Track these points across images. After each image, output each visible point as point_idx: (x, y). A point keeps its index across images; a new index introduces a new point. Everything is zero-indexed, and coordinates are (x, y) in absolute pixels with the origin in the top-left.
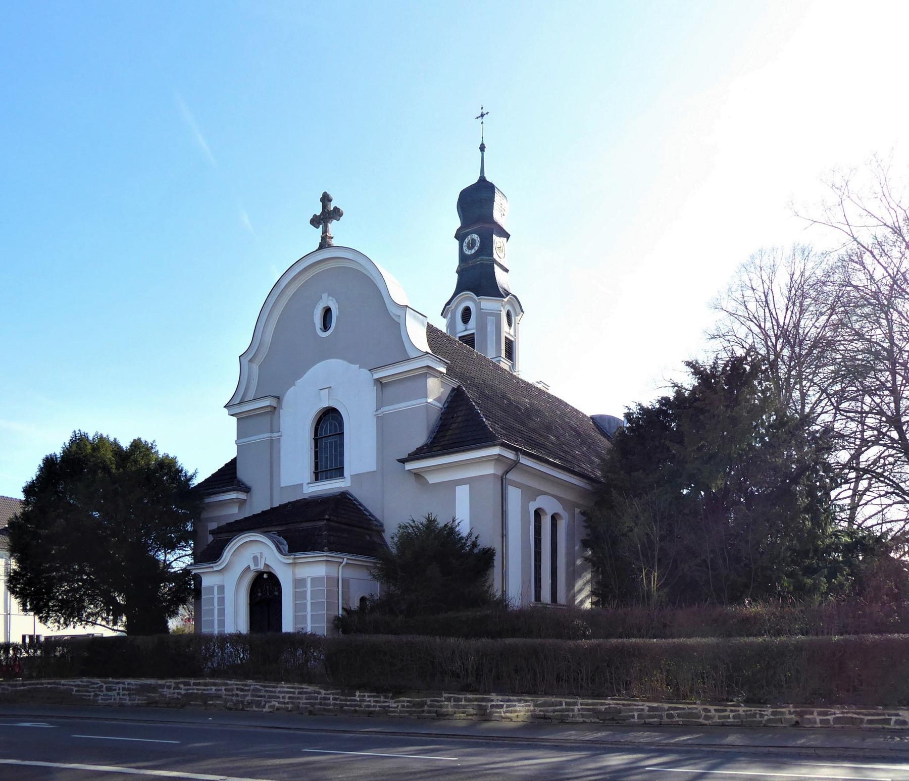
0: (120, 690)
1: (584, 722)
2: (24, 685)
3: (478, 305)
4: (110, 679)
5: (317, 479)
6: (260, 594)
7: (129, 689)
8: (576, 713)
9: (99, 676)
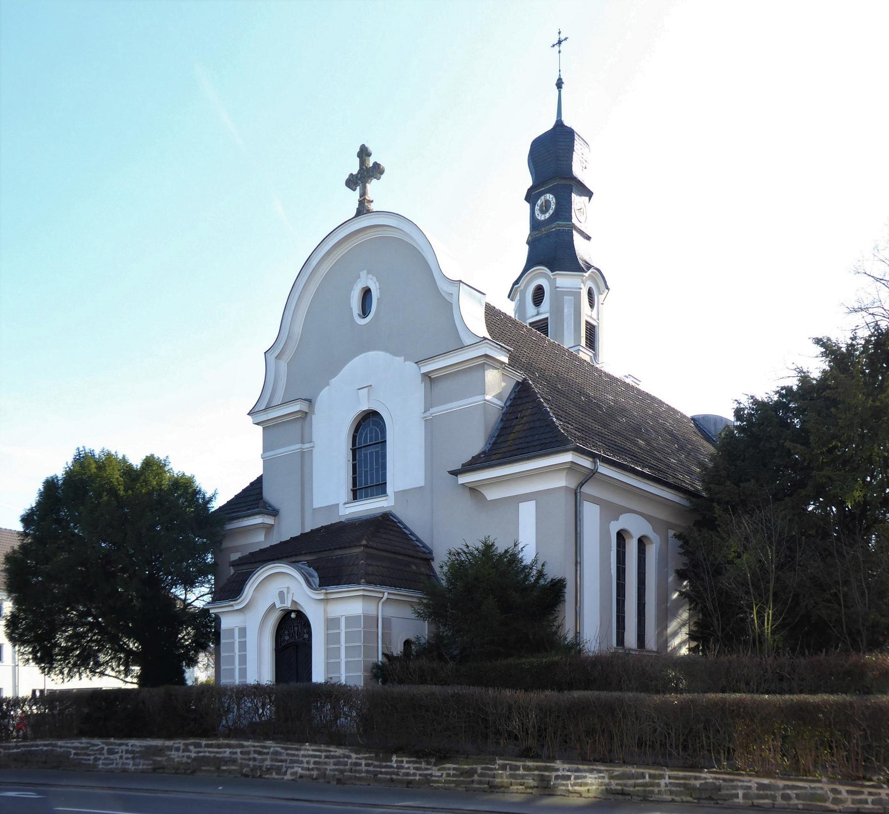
0: (123, 752)
1: (673, 801)
2: (17, 747)
3: (552, 283)
4: (112, 740)
5: (355, 498)
7: (132, 752)
8: (663, 788)
9: (100, 736)
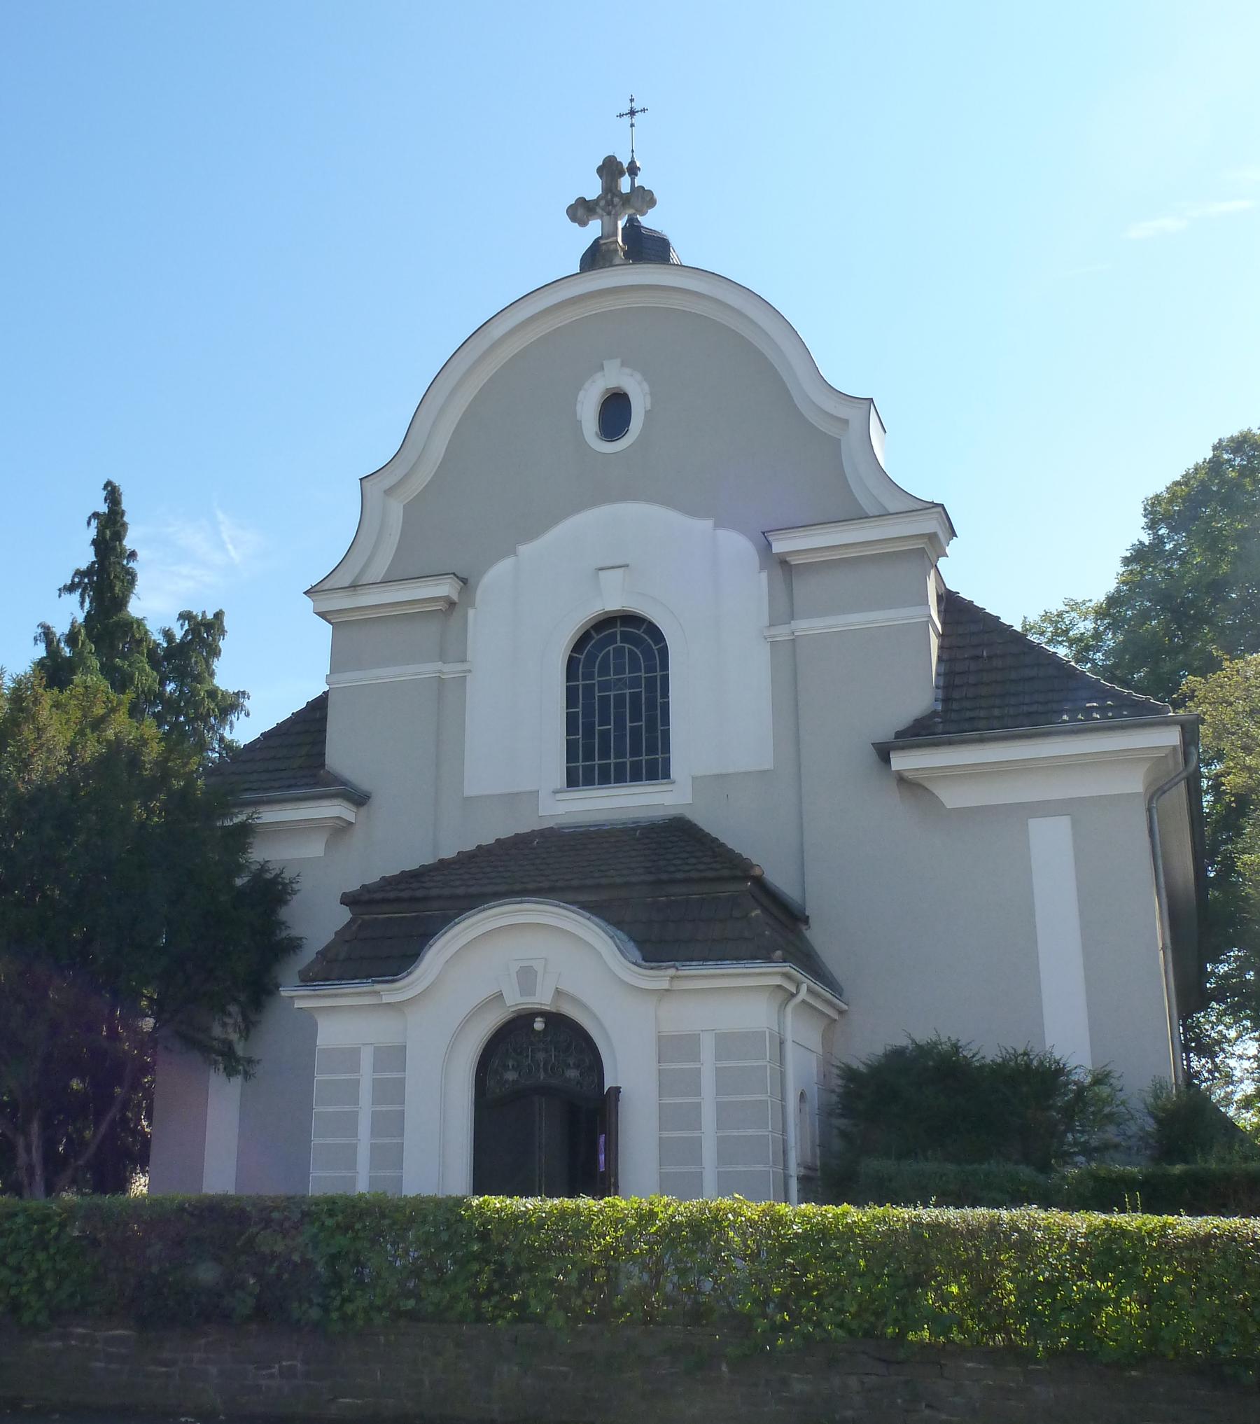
6: (511, 1076)
